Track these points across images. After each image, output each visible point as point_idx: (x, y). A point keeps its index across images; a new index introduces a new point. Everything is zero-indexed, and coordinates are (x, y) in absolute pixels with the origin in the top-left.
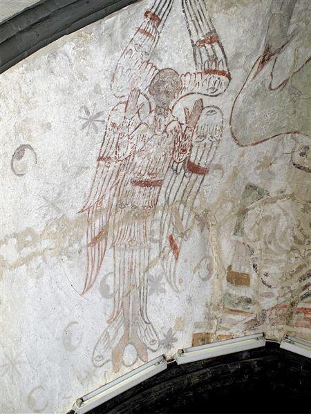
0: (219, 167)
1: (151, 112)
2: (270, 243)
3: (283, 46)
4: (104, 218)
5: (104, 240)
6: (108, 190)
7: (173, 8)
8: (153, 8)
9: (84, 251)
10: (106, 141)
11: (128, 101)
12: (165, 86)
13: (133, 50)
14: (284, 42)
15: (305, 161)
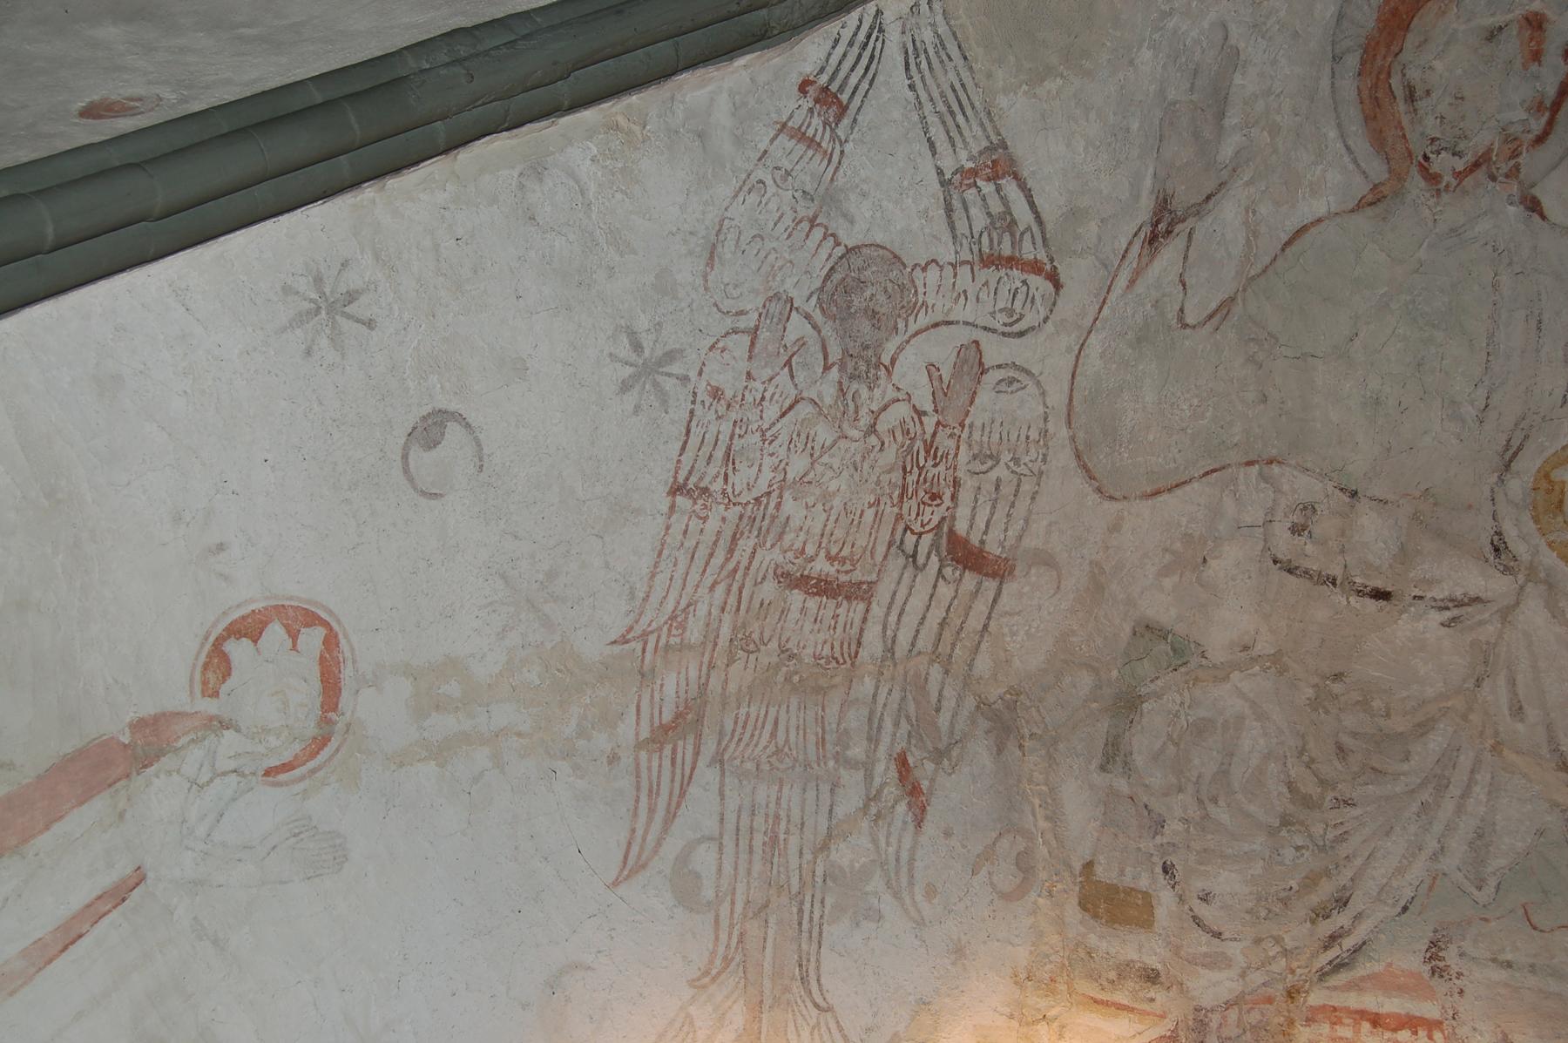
0: (1045, 560)
1: (827, 368)
2: (1215, 800)
3: (1208, 198)
4: (693, 674)
5: (691, 739)
6: (703, 591)
7: (880, 78)
8: (822, 70)
9: (627, 760)
10: (694, 441)
11: (757, 328)
12: (868, 293)
13: (769, 182)
14: (1210, 186)
15: (1309, 548)
